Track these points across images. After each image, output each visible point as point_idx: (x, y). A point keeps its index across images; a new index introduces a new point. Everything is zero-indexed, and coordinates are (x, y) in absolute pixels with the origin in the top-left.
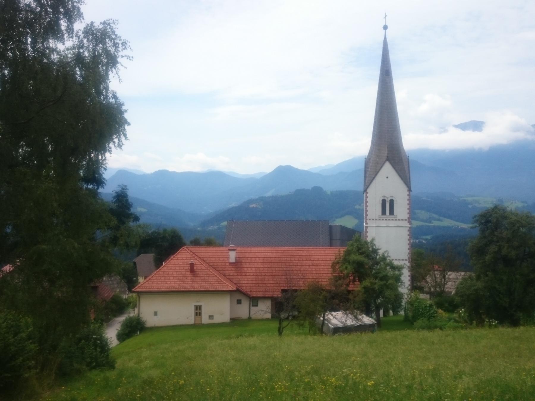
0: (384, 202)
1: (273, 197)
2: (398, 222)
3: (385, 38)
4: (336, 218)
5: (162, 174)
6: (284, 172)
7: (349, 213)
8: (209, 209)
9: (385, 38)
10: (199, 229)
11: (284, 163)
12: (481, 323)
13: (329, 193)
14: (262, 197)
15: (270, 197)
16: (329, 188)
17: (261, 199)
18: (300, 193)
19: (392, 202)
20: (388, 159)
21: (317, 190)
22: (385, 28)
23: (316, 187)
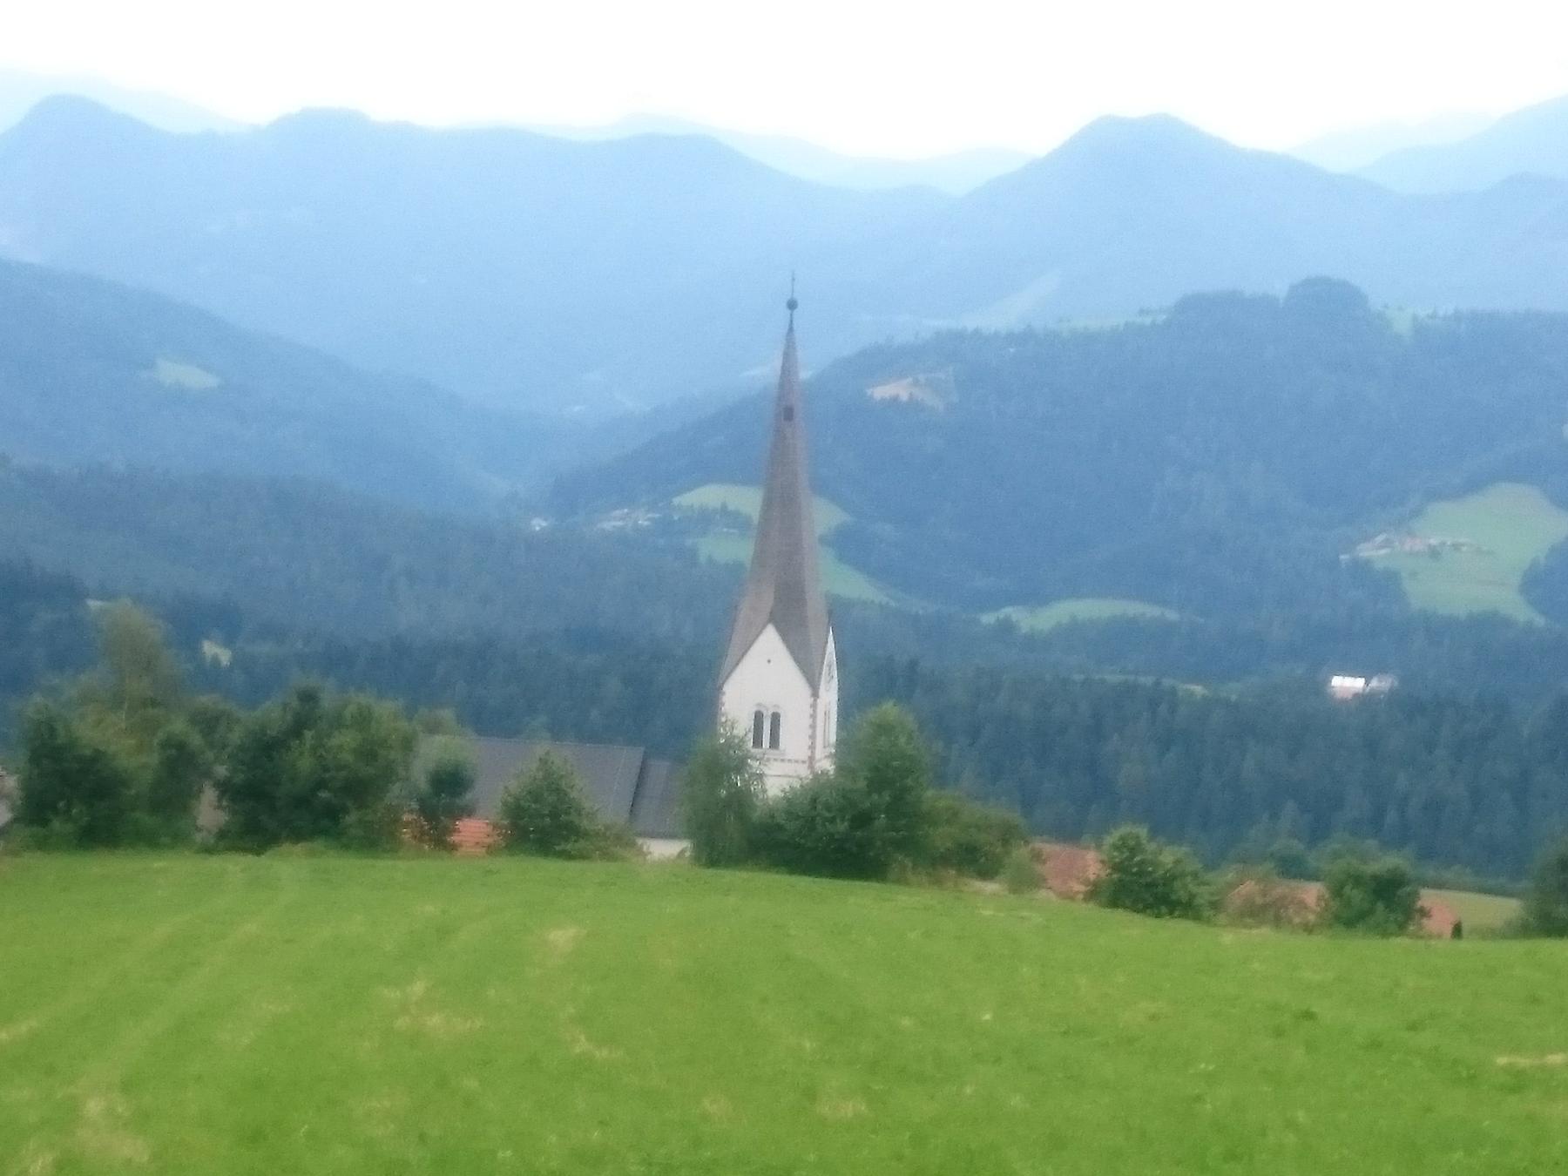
0: (759, 717)
1: (1024, 338)
2: (786, 764)
3: (791, 329)
4: (1435, 495)
5: (321, 141)
6: (1134, 165)
7: (1519, 471)
8: (620, 387)
9: (791, 329)
10: (538, 524)
11: (1134, 99)
12: (43, 845)
13: (1402, 324)
14: (959, 336)
15: (1011, 338)
16: (1412, 291)
17: (952, 348)
18: (1209, 317)
19: (776, 718)
20: (773, 619)
21: (1329, 306)
22: (792, 305)
23: (1309, 283)
